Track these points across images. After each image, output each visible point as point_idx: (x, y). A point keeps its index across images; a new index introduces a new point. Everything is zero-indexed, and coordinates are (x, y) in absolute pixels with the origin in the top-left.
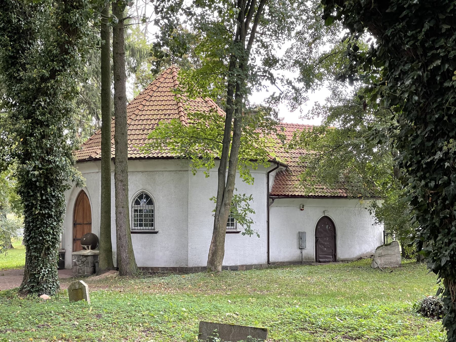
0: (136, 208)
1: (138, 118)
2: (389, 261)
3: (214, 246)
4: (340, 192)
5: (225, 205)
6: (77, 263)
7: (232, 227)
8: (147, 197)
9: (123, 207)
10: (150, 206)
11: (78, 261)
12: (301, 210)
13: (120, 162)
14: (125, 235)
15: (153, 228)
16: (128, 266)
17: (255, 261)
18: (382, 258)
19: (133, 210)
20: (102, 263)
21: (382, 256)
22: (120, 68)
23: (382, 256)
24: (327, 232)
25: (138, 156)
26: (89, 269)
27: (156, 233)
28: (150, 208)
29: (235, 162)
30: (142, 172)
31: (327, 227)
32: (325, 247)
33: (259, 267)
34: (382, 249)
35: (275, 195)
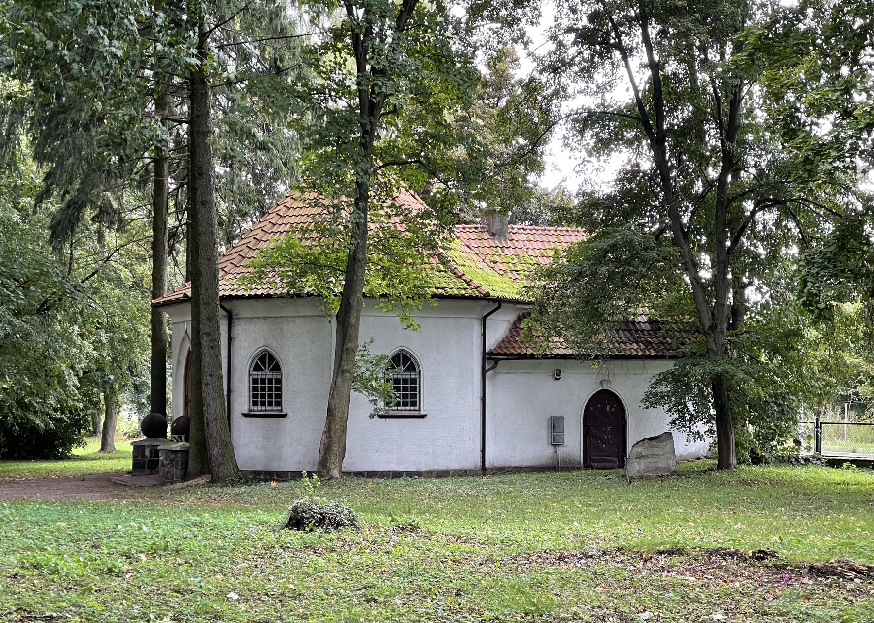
0: (256, 377)
1: (275, 229)
2: (654, 465)
3: (327, 438)
4: (633, 348)
5: (343, 372)
6: (165, 463)
7: (412, 408)
8: (272, 358)
9: (211, 376)
10: (412, 373)
11: (166, 459)
12: (556, 379)
13: (205, 304)
14: (216, 419)
15: (279, 408)
16: (222, 469)
17: (454, 465)
18: (642, 461)
19: (251, 379)
20: (192, 465)
21: (643, 457)
22: (203, 155)
23: (643, 457)
24: (605, 420)
25: (253, 293)
26: (177, 472)
27: (284, 416)
28: (413, 377)
29: (355, 304)
30: (264, 318)
31: (608, 409)
32: (603, 443)
33: (463, 473)
34: (643, 445)
35: (499, 354)
